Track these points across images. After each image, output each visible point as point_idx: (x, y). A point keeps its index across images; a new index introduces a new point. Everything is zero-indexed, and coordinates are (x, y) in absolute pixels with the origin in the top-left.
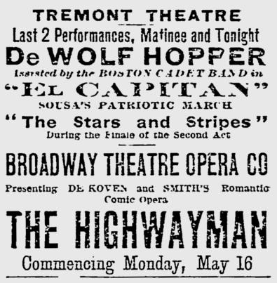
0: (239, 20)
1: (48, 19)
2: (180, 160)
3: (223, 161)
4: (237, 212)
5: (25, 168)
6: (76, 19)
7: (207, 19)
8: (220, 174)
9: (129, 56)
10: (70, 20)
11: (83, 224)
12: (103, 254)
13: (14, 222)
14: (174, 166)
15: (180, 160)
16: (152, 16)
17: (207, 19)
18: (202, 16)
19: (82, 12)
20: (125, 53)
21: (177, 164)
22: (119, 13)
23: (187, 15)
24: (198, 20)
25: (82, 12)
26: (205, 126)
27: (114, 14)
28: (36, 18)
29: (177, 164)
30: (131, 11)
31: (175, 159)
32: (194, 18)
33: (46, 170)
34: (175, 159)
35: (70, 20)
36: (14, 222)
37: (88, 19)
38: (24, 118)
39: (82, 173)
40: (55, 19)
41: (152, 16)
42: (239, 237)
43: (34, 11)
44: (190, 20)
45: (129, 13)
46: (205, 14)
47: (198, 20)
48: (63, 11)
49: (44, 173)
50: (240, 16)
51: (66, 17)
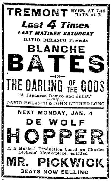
0: (40, 124)
1: (16, 14)
2: (23, 83)
3: (40, 84)
4: (19, 142)
5: (42, 87)
6: (33, 15)
7: (35, 172)
8: (49, 90)
9: (83, 123)
10: (29, 15)
11: (14, 83)
12: (43, 93)
13: (8, 82)
14: (20, 86)
15: (23, 83)
16: (34, 171)
17: (35, 172)
18: (33, 171)
19: (40, 112)
20: (82, 122)
21: (21, 85)
22: (60, 11)
23: (28, 171)
24: (60, 114)
25: (40, 112)
26: (31, 15)
27: (11, 159)
28: (58, 121)
29: (21, 85)
30: (34, 111)
31: (21, 82)
32: (47, 51)
33: (35, 88)
34: (21, 82)
35: (29, 15)
36: (8, 82)
37: (40, 15)
38: (7, 79)
39: (34, 90)
40: (20, 15)
41: (34, 171)
42: (34, 88)
43: (67, 87)
44: (45, 52)
45: (66, 12)
46: (63, 11)
47: (60, 114)
48: (23, 111)
49: (34, 90)
50: (41, 122)
51: (81, 51)
